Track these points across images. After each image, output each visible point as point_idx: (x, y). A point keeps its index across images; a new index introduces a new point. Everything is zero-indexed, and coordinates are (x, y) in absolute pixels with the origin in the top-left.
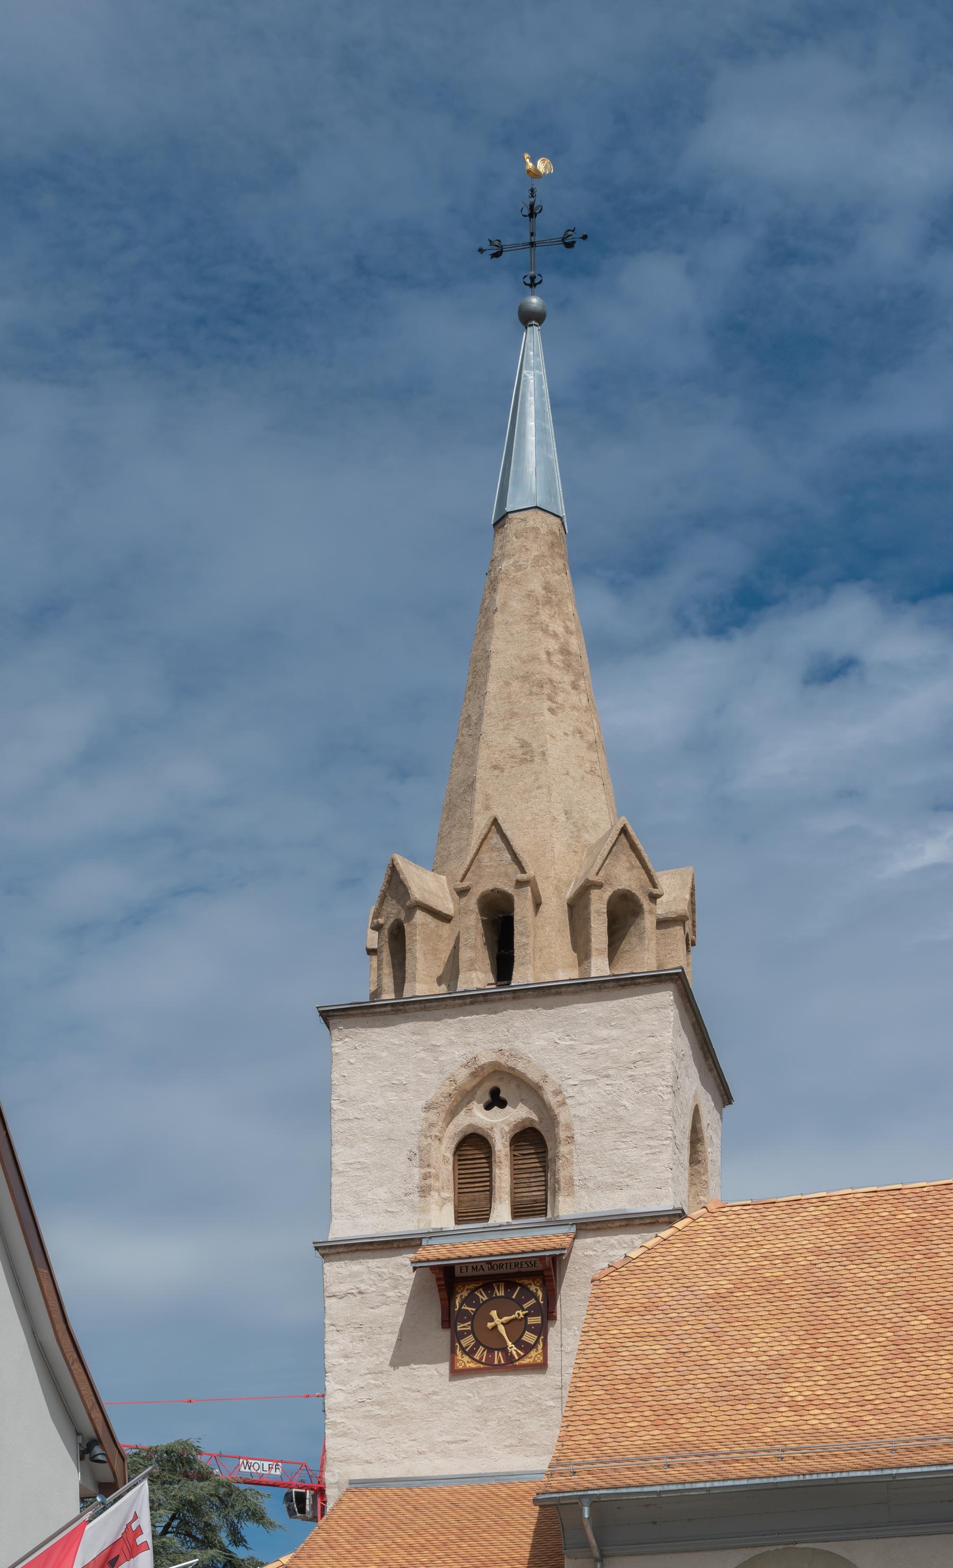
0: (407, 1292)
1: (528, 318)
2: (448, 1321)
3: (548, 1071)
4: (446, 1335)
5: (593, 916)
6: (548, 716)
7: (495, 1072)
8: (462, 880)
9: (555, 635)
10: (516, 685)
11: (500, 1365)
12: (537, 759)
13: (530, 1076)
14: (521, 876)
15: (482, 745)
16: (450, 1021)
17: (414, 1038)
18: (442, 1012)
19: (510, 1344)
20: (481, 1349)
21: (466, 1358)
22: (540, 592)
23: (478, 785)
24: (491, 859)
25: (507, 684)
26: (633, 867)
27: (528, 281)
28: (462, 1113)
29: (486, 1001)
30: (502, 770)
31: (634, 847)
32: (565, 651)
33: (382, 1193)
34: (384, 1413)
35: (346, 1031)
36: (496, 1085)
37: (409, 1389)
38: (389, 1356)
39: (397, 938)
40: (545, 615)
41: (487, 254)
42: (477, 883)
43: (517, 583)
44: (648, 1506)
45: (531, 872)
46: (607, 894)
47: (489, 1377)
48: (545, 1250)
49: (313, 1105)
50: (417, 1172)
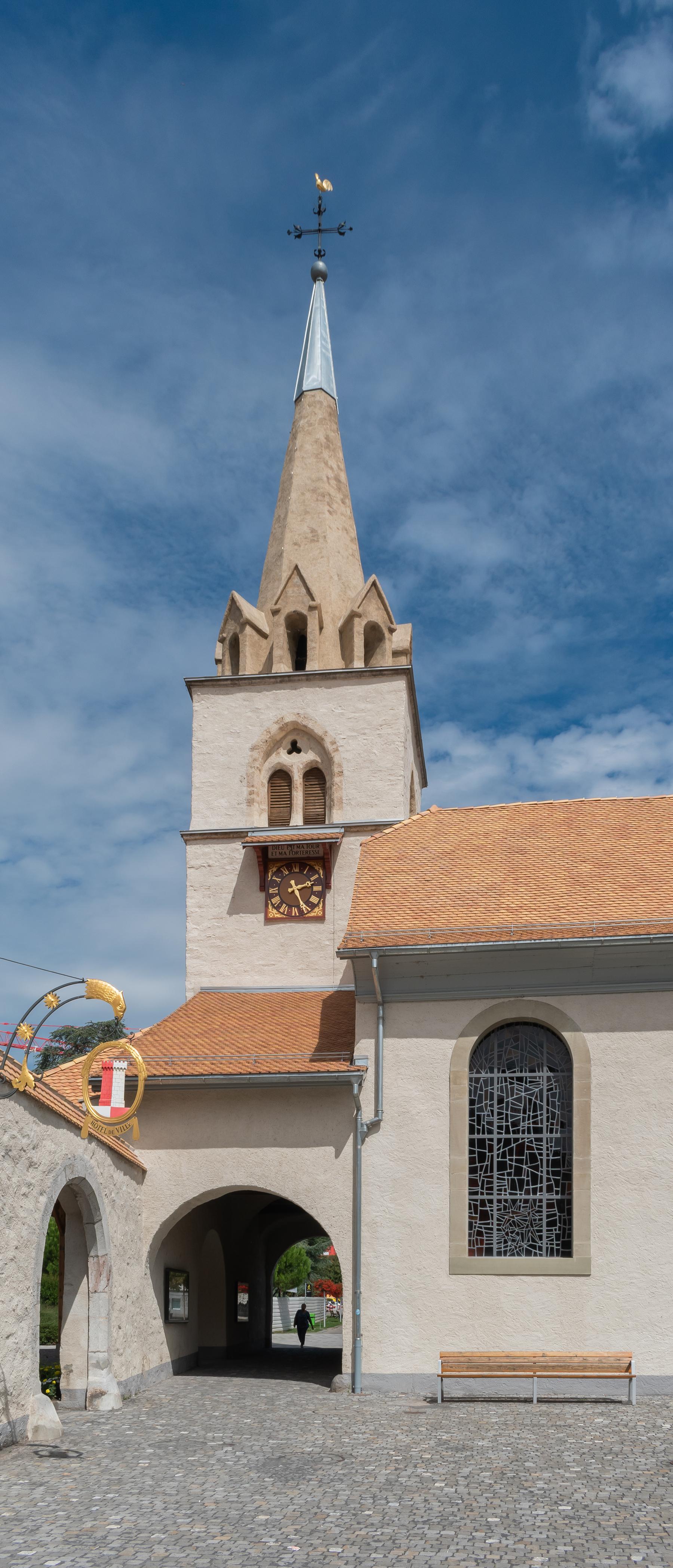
0: (238, 867)
1: (317, 275)
2: (263, 887)
3: (328, 729)
4: (262, 895)
5: (356, 635)
6: (327, 515)
7: (295, 729)
8: (276, 604)
9: (332, 468)
10: (308, 495)
11: (296, 916)
12: (321, 540)
13: (316, 731)
14: (312, 603)
15: (287, 530)
16: (267, 693)
17: (245, 703)
18: (262, 687)
19: (301, 903)
20: (284, 905)
21: (275, 911)
22: (323, 440)
23: (285, 554)
24: (293, 592)
25: (303, 494)
26: (379, 608)
27: (317, 253)
28: (274, 755)
29: (290, 681)
30: (300, 546)
31: (380, 596)
32: (337, 479)
33: (223, 802)
34: (223, 944)
35: (202, 696)
36: (296, 738)
37: (239, 930)
38: (227, 908)
39: (234, 647)
40: (326, 454)
41: (292, 236)
42: (285, 607)
43: (310, 434)
44: (418, 962)
45: (318, 601)
46: (364, 623)
47: (289, 924)
48: (326, 839)
49: (181, 739)
50: (245, 790)
